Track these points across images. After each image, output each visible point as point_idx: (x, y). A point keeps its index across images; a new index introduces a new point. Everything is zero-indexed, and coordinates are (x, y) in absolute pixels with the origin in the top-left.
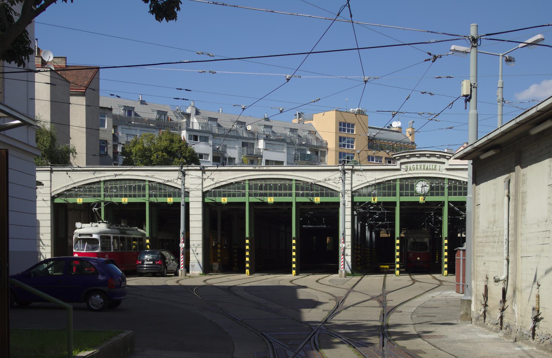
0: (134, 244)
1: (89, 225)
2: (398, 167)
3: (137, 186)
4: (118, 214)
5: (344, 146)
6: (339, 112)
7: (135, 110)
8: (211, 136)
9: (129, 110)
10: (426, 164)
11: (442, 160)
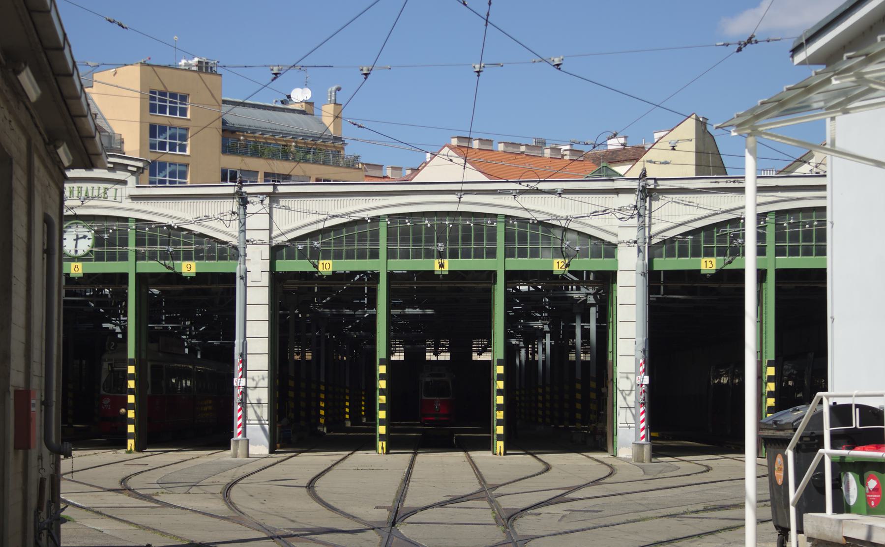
5: (162, 146)
6: (150, 68)
10: (84, 186)
11: (120, 175)
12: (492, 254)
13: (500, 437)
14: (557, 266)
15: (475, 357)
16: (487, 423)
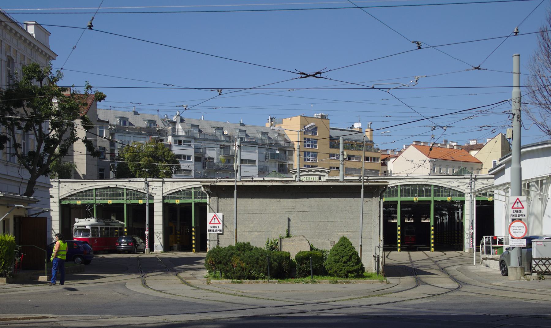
0: (117, 232)
1: (84, 220)
2: (294, 179)
3: (117, 192)
4: (105, 212)
5: (308, 146)
7: (129, 120)
8: (193, 141)
9: (124, 120)
12: (430, 196)
13: (432, 247)
14: (449, 199)
15: (422, 221)
16: (429, 245)
